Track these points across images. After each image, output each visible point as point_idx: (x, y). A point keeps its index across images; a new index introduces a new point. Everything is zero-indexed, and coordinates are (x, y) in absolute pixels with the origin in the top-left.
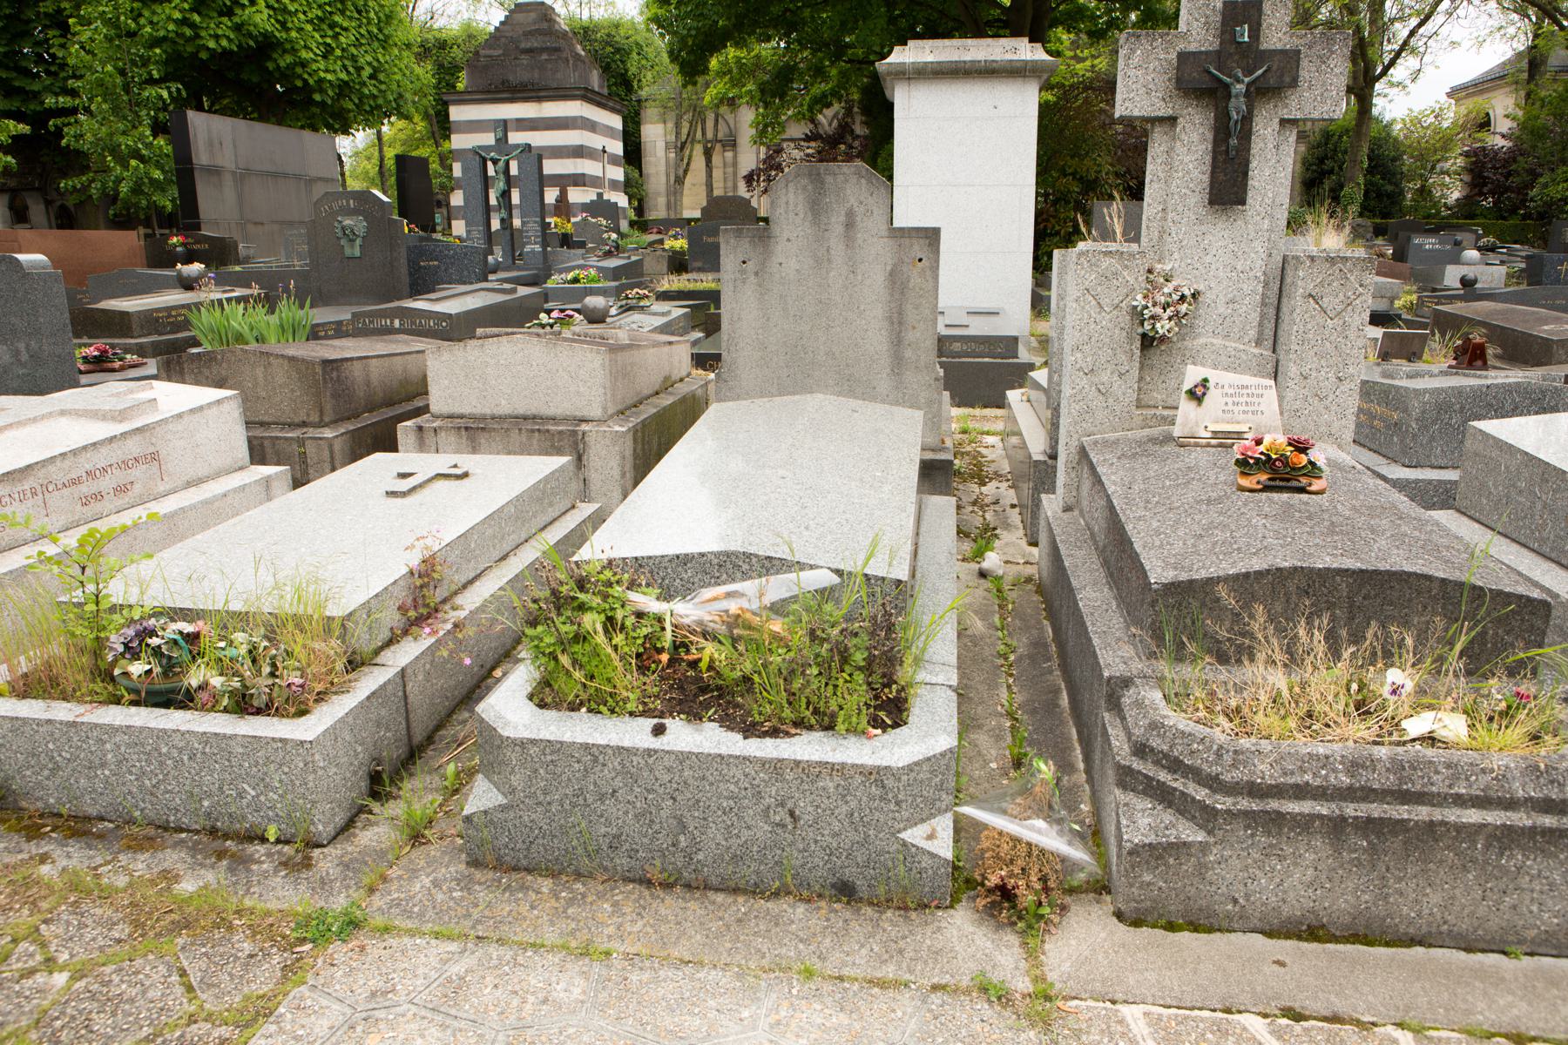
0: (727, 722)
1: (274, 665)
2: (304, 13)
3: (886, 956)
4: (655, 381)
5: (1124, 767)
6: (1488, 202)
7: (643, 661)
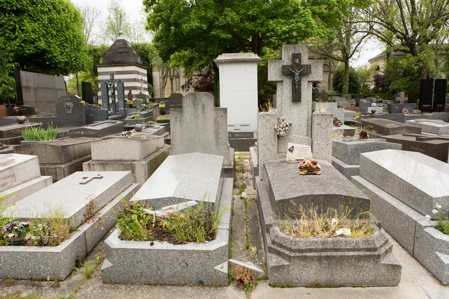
0: (170, 241)
1: (49, 232)
2: (55, 43)
4: (154, 149)
6: (380, 89)
7: (148, 226)
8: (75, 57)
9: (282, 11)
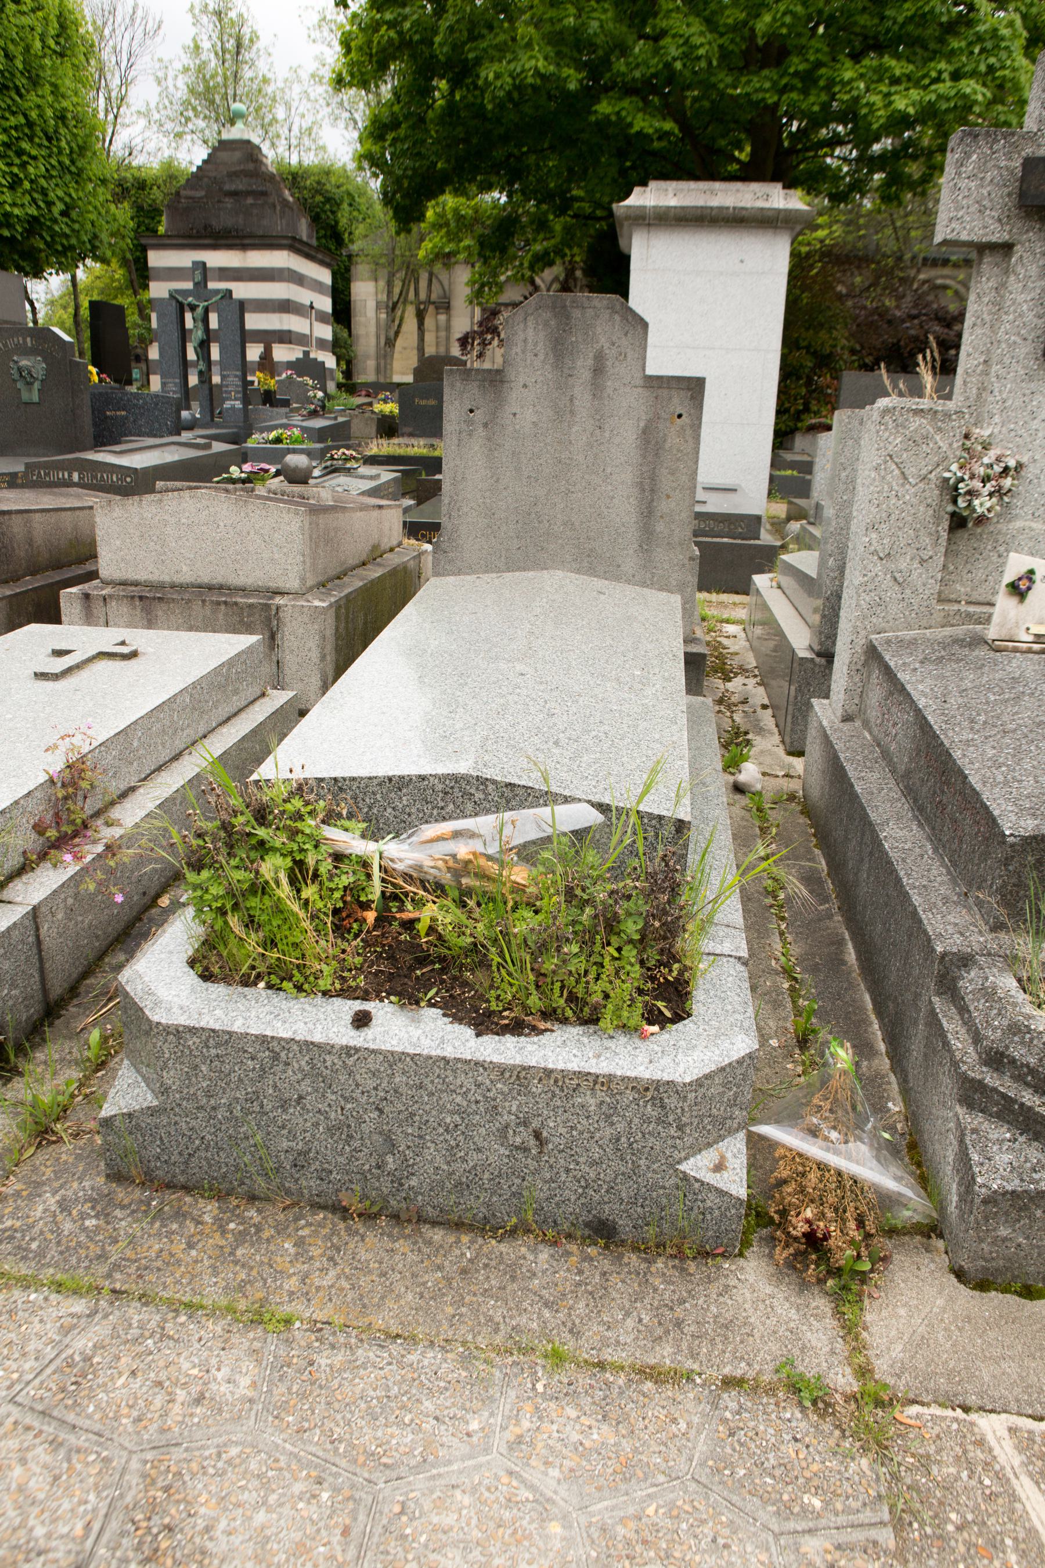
3: (659, 1331)
5: (973, 1080)
7: (343, 919)
8: (66, 204)
9: (900, 19)
